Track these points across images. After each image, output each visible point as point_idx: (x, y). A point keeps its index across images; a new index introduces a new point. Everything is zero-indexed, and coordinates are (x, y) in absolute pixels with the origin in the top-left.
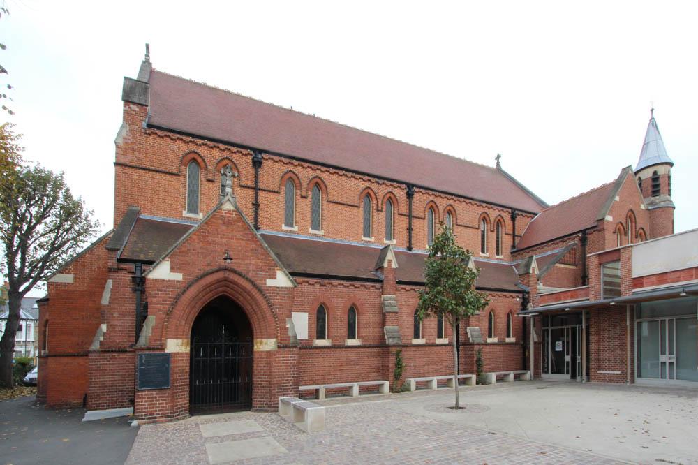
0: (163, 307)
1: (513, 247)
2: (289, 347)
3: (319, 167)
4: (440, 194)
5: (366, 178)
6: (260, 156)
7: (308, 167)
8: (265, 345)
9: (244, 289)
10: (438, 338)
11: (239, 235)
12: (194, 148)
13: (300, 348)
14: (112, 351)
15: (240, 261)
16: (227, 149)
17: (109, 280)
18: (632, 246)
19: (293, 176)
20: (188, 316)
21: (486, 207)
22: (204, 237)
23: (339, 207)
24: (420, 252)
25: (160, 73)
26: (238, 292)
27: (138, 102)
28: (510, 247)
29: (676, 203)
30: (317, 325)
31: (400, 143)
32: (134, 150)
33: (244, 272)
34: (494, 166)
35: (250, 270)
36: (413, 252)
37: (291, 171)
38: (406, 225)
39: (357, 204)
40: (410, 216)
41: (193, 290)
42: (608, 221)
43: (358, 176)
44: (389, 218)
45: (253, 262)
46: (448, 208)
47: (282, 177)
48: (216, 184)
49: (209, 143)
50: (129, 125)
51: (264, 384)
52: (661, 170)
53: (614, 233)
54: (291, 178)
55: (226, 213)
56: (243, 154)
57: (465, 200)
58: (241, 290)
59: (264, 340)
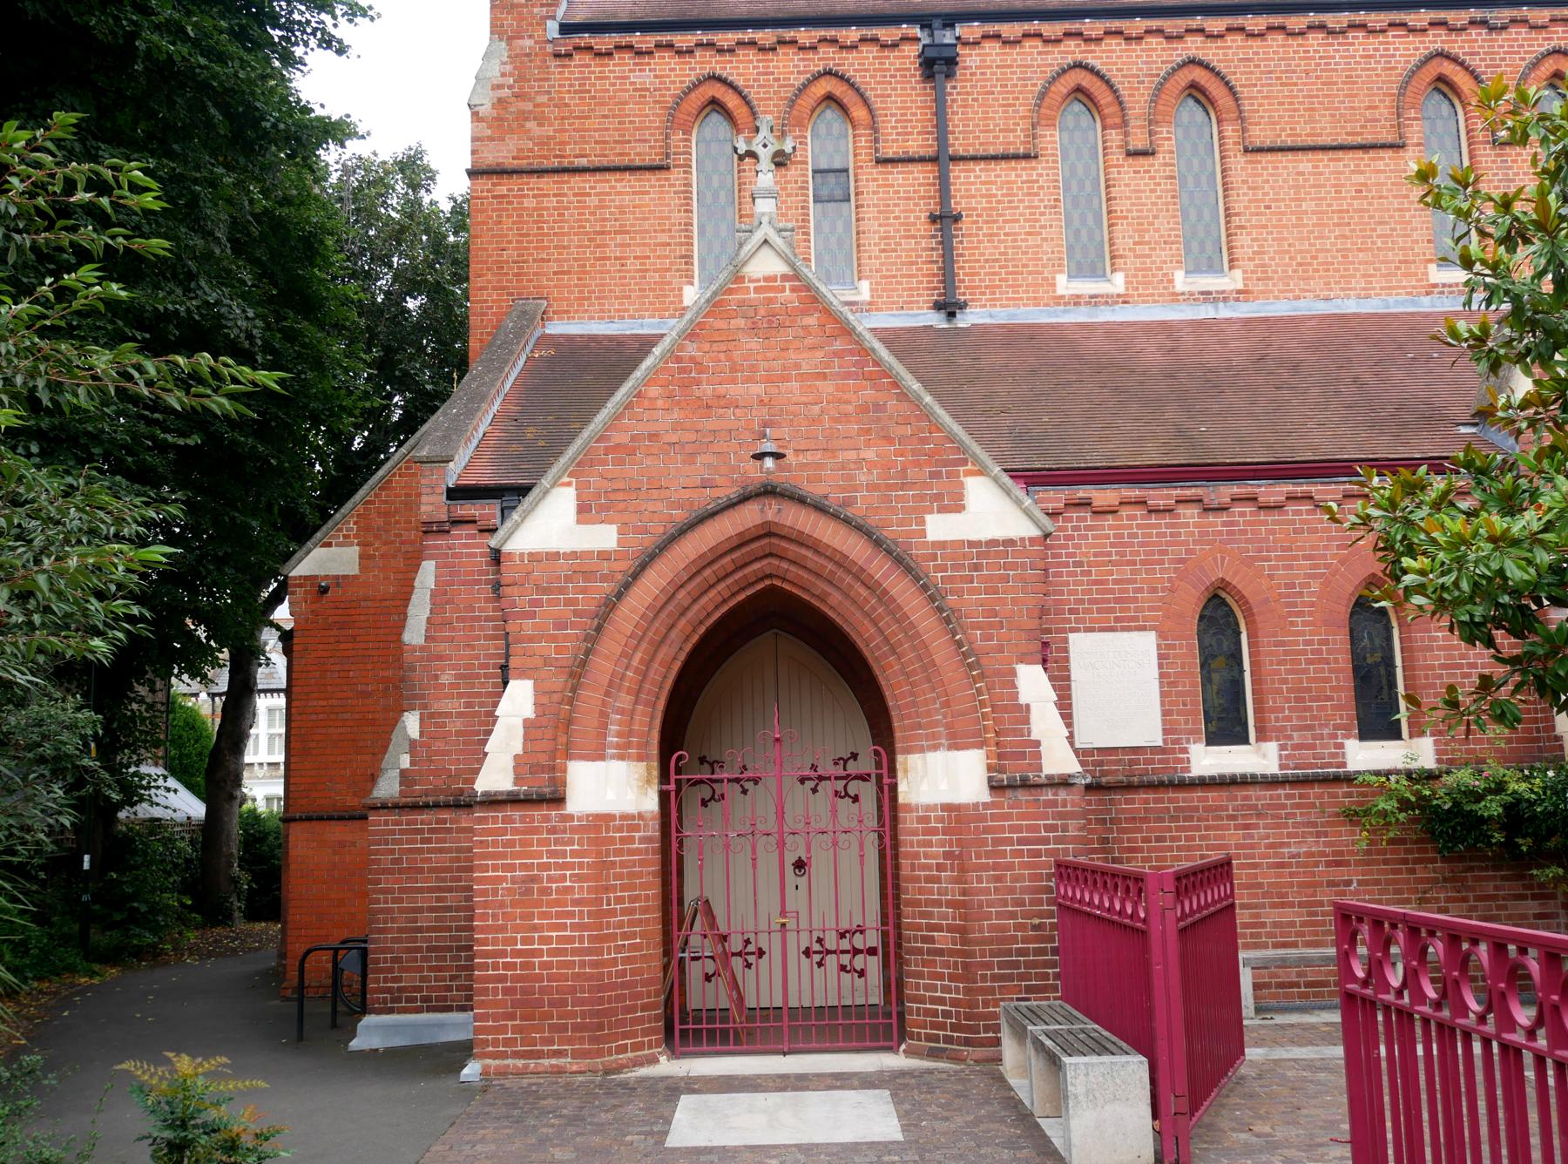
0: (558, 650)
6: (948, 38)
9: (841, 561)
11: (809, 362)
14: (437, 806)
15: (818, 457)
17: (424, 563)
19: (1086, 80)
20: (645, 675)
22: (685, 385)
23: (1305, 163)
26: (818, 575)
30: (1207, 680)
32: (523, 116)
33: (835, 498)
35: (855, 489)
37: (1078, 65)
39: (1389, 138)
41: (654, 582)
45: (870, 454)
47: (1042, 95)
50: (510, 39)
51: (943, 940)
54: (1079, 89)
55: (757, 290)
58: (830, 566)
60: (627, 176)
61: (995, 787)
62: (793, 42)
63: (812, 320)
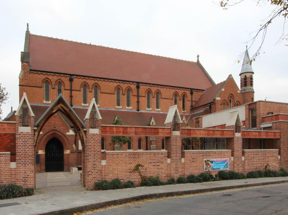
1: (192, 106)
2: (74, 153)
3: (97, 79)
4: (153, 85)
5: (117, 81)
7: (92, 79)
8: (67, 152)
9: (60, 136)
10: (162, 149)
12: (47, 76)
13: (78, 153)
16: (59, 75)
18: (202, 117)
21: (177, 89)
23: (106, 95)
24: (143, 112)
25: (33, 35)
27: (26, 61)
28: (190, 107)
29: (255, 90)
31: (144, 54)
32: (25, 79)
34: (196, 61)
36: (140, 111)
38: (136, 100)
39: (113, 93)
40: (138, 96)
41: (45, 137)
42: (218, 100)
43: (113, 81)
44: (128, 97)
46: (157, 91)
48: (56, 89)
49: (52, 74)
50: (24, 70)
52: (248, 75)
53: (221, 105)
56: (66, 77)
57: (165, 87)
59: (67, 150)
60: (37, 88)
61: (71, 152)
62: (56, 75)
63: (58, 117)
